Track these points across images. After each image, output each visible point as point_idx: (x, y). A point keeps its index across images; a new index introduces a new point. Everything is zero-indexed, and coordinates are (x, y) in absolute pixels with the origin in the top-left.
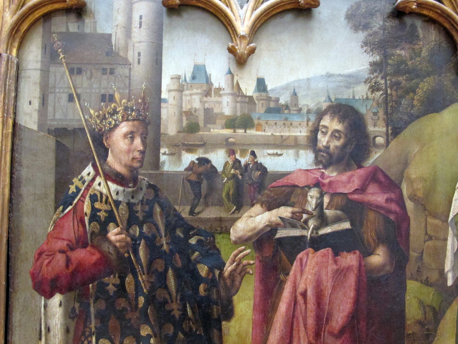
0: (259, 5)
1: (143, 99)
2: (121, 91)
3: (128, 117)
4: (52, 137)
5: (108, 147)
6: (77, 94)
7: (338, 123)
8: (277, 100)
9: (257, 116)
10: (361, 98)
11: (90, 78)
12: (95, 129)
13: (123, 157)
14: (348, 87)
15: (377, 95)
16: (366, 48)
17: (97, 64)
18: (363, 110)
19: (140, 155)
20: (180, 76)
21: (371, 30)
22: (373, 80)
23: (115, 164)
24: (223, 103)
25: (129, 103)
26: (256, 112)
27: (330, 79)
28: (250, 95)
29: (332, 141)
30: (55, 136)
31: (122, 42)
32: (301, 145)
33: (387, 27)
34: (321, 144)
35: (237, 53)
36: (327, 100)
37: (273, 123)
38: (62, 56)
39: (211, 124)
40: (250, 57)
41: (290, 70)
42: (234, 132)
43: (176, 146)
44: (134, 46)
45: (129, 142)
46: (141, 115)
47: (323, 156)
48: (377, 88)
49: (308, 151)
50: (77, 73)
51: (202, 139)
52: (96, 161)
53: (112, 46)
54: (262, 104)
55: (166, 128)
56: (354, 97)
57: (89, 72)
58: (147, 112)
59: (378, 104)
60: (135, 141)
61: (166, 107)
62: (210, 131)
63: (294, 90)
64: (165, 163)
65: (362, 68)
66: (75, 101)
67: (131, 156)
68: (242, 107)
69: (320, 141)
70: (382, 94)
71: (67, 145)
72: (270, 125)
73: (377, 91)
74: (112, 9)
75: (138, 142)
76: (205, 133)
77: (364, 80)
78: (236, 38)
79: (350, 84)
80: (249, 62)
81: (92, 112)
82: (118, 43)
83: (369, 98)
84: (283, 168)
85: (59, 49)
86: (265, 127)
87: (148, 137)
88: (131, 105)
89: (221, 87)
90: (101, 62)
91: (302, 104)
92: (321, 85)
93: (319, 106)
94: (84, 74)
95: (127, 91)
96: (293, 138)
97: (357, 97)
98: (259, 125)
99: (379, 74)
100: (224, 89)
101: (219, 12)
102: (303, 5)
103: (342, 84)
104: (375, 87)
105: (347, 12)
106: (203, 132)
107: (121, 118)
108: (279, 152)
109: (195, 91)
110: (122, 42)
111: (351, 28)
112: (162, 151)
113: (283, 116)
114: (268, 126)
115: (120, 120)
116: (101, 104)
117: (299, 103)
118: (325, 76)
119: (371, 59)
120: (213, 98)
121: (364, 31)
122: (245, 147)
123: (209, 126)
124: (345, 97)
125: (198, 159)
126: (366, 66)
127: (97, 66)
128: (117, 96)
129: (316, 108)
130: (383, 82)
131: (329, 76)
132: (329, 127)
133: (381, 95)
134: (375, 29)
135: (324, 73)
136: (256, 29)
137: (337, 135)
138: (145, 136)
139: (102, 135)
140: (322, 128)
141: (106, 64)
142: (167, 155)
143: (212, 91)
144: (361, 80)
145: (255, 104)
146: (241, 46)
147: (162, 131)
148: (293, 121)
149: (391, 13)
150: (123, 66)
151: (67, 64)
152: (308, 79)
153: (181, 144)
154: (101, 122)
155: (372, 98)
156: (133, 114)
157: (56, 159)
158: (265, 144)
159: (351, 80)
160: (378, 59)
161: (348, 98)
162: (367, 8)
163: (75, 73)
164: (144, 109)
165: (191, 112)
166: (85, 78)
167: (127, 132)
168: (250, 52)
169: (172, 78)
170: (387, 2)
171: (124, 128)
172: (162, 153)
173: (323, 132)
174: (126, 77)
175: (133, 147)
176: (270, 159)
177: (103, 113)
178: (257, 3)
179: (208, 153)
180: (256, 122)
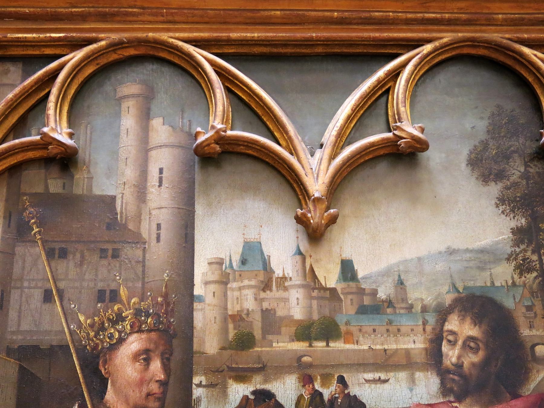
0: (338, 151)
1: (166, 296)
2: (130, 284)
3: (141, 326)
4: (12, 360)
5: (106, 376)
6: (58, 290)
7: (473, 325)
8: (374, 293)
9: (345, 320)
10: (504, 284)
11: (81, 264)
12: (86, 346)
13: (131, 393)
14: (481, 269)
15: (529, 279)
16: (504, 207)
17: (93, 242)
18: (509, 303)
19: (160, 388)
20: (222, 259)
21: (508, 180)
22: (520, 255)
23: (119, 405)
24: (290, 301)
25: (142, 303)
26: (342, 313)
27: (452, 258)
28: (331, 287)
29: (466, 355)
30: (19, 360)
31: (131, 209)
32: (417, 363)
33: (531, 174)
34: (449, 361)
35: (311, 223)
36: (451, 290)
37: (370, 329)
38: (36, 230)
39: (273, 333)
40: (328, 228)
41: (390, 246)
42: (311, 346)
43: (218, 371)
44: (150, 214)
45: (142, 367)
46: (161, 323)
47: (453, 380)
48: (527, 268)
49: (429, 373)
50: (60, 257)
51: (259, 358)
52: (85, 400)
53: (117, 214)
54: (351, 300)
55: (202, 342)
56: (493, 283)
57: (78, 255)
58: (172, 317)
59: (532, 293)
60: (151, 365)
61: (202, 309)
62: (271, 346)
63: (399, 276)
64: (200, 401)
65: (501, 238)
66: (55, 301)
67: (145, 390)
68: (320, 306)
69: (447, 355)
70: (537, 276)
71: (39, 375)
72: (366, 332)
73: (528, 272)
74: (117, 160)
75: (156, 365)
76: (264, 349)
77: (507, 256)
78: (308, 201)
79: (485, 263)
80: (327, 235)
81: (82, 318)
82: (126, 209)
83: (517, 284)
84: (392, 402)
85: (33, 218)
86: (358, 337)
87: (172, 358)
88: (146, 307)
89: (286, 275)
90: (99, 239)
91: (414, 297)
92: (440, 266)
93: (439, 300)
94: (71, 258)
95: (140, 285)
96: (404, 351)
97: (497, 284)
98: (349, 334)
99: (527, 246)
100: (291, 278)
101: (279, 162)
102: (404, 150)
103: (471, 264)
104: (524, 266)
105: (469, 156)
106: (262, 347)
107: (129, 327)
108: (383, 376)
109: (246, 282)
110: (131, 209)
111: (477, 178)
112: (196, 380)
113: (385, 318)
114: (363, 336)
115: (128, 332)
116: (97, 304)
117: (409, 295)
118: (445, 252)
119: (513, 224)
120: (275, 293)
121: (498, 182)
122: (327, 371)
123: (270, 337)
124: (479, 283)
125: (254, 393)
126: (507, 235)
127: (92, 246)
128: (123, 293)
129: (435, 303)
130: (535, 257)
131: (451, 252)
132: (459, 333)
133: (536, 278)
134: (514, 178)
135: (443, 248)
136: (335, 186)
137: (472, 344)
138: (167, 356)
139: (98, 357)
140: (447, 336)
141: (108, 242)
142: (204, 386)
143: (272, 281)
144: (502, 256)
145: (340, 300)
146: (315, 215)
147: (196, 347)
148: (401, 325)
149: (534, 153)
150: (134, 245)
151: (44, 242)
152: (419, 259)
153: (226, 369)
154: (97, 334)
155: (521, 283)
156: (149, 320)
157: (18, 399)
158: (359, 365)
159: (486, 257)
160: (524, 223)
161: (483, 285)
162: (498, 148)
163: (57, 256)
164: (166, 313)
165: (240, 316)
166: (71, 264)
167: (139, 351)
168: (329, 221)
169: (210, 264)
170: (527, 139)
171: (133, 344)
172: (195, 385)
173: (449, 341)
174: (138, 262)
175: (149, 375)
176: (370, 390)
177: (100, 320)
178: (335, 149)
179: (270, 381)
180: (343, 328)
